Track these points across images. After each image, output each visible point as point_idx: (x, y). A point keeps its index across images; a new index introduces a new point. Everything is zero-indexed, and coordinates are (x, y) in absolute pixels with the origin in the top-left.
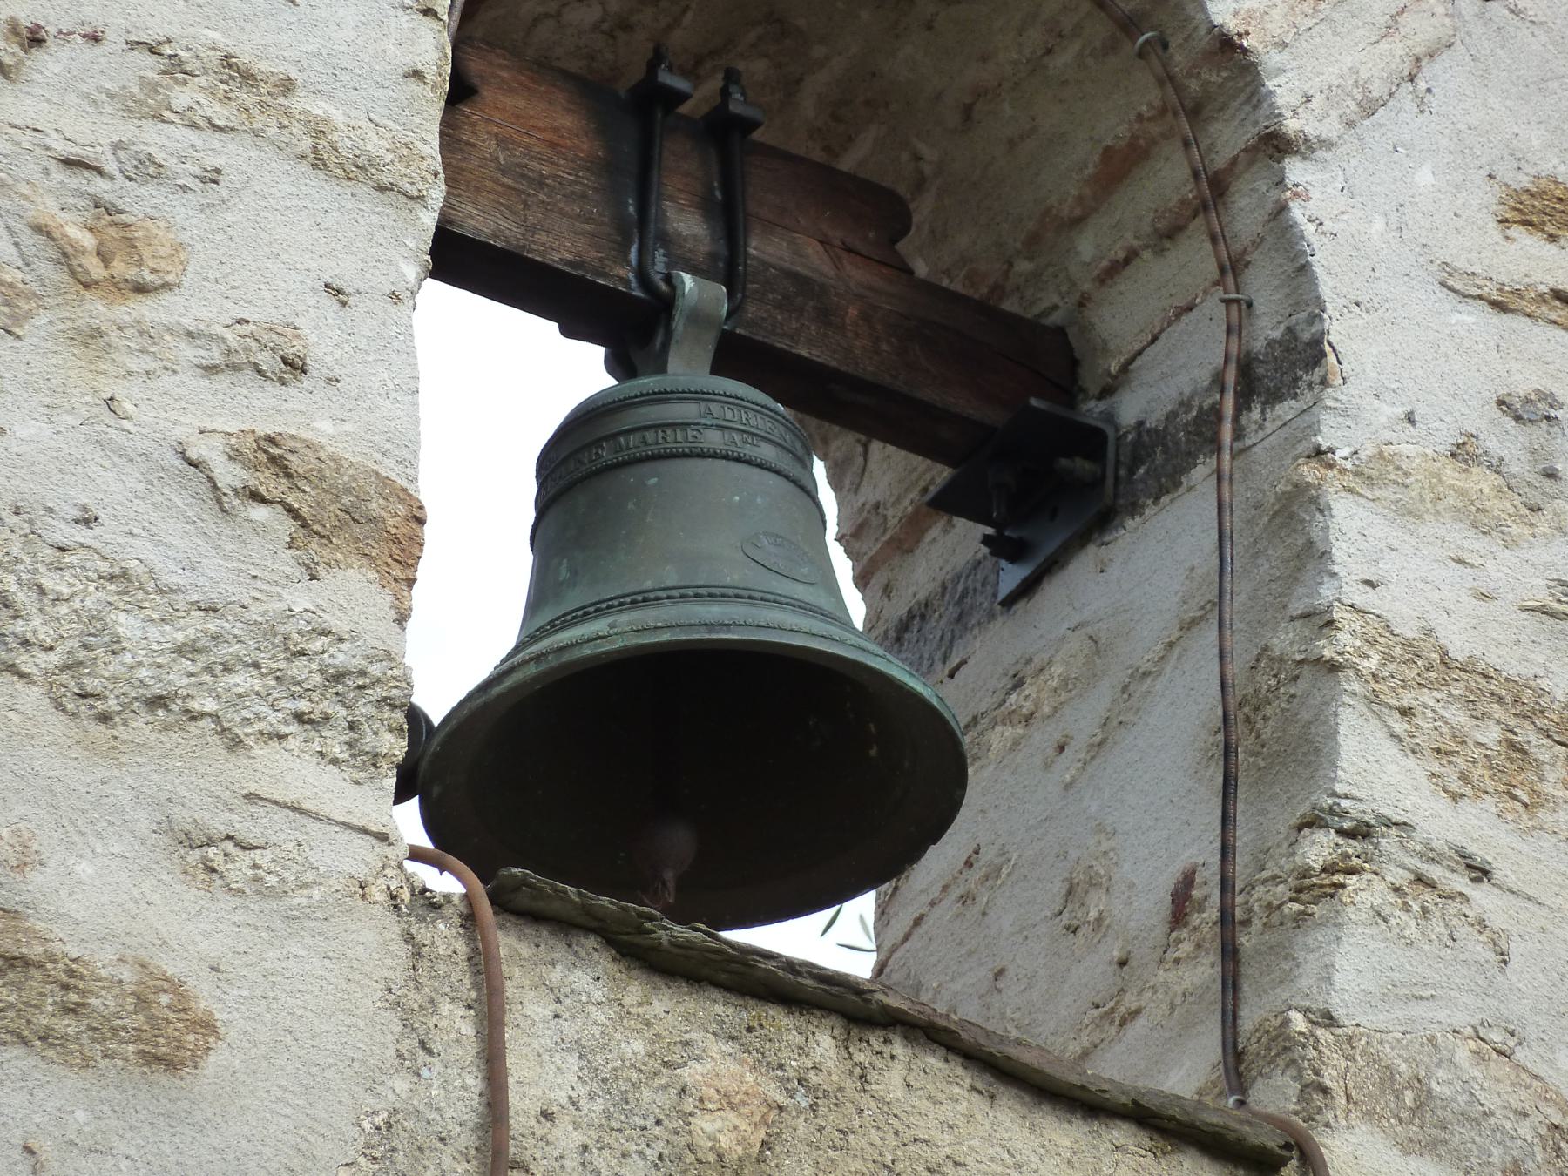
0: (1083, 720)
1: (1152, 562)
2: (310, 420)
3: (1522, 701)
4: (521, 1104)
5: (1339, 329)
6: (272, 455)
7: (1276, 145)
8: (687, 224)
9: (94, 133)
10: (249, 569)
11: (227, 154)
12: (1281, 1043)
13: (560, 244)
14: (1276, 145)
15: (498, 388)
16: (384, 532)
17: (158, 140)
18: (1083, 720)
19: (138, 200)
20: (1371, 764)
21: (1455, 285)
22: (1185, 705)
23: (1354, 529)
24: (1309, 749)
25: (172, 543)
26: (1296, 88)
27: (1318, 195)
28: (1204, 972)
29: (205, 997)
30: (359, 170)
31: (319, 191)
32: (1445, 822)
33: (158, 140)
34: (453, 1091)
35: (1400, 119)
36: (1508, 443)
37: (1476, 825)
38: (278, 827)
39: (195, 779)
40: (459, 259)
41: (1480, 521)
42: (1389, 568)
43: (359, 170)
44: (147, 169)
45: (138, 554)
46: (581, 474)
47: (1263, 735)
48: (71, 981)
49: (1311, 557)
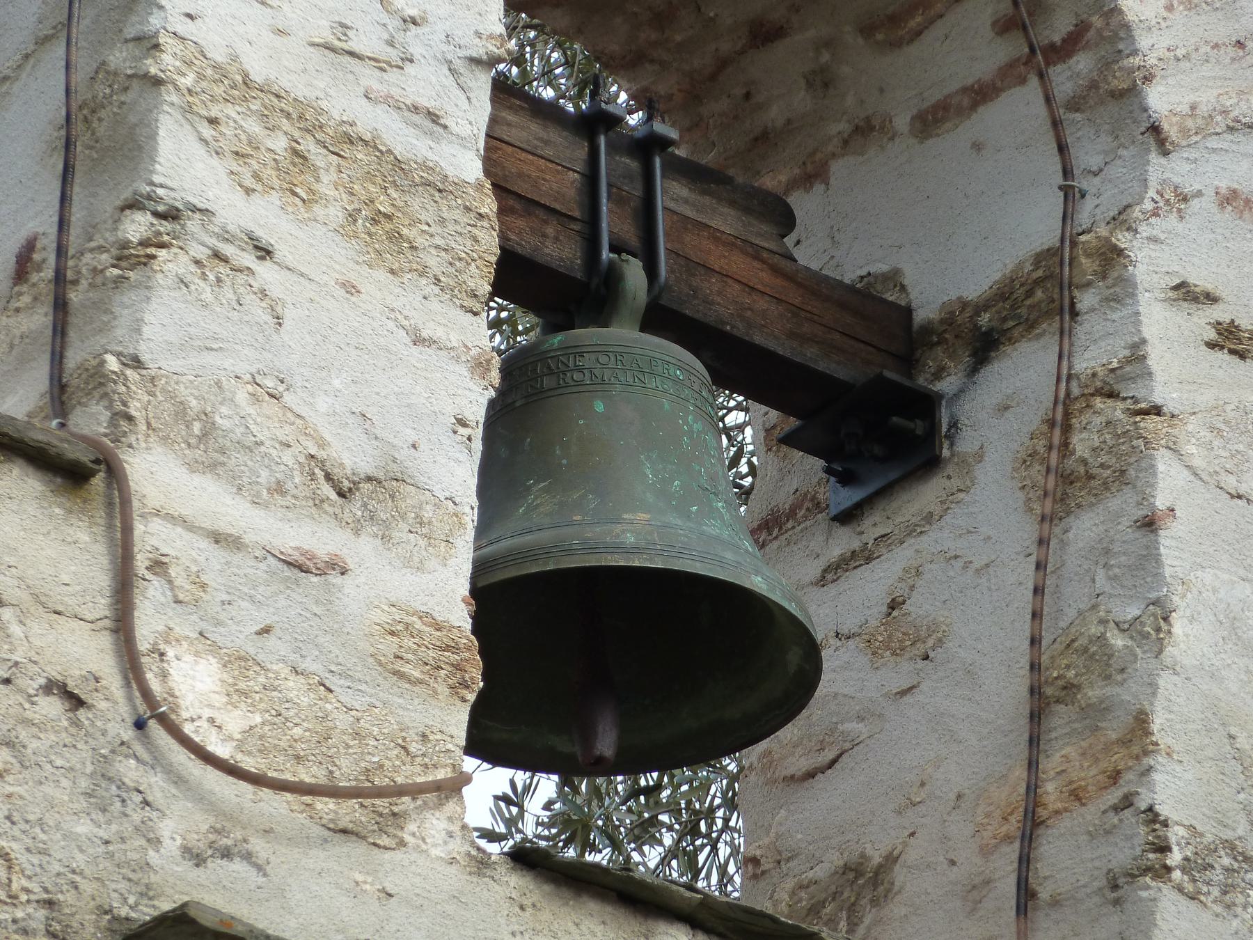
3: (306, 118)
12: (98, 379)
20: (182, 161)
24: (134, 147)
28: (40, 319)
32: (237, 210)
37: (264, 214)
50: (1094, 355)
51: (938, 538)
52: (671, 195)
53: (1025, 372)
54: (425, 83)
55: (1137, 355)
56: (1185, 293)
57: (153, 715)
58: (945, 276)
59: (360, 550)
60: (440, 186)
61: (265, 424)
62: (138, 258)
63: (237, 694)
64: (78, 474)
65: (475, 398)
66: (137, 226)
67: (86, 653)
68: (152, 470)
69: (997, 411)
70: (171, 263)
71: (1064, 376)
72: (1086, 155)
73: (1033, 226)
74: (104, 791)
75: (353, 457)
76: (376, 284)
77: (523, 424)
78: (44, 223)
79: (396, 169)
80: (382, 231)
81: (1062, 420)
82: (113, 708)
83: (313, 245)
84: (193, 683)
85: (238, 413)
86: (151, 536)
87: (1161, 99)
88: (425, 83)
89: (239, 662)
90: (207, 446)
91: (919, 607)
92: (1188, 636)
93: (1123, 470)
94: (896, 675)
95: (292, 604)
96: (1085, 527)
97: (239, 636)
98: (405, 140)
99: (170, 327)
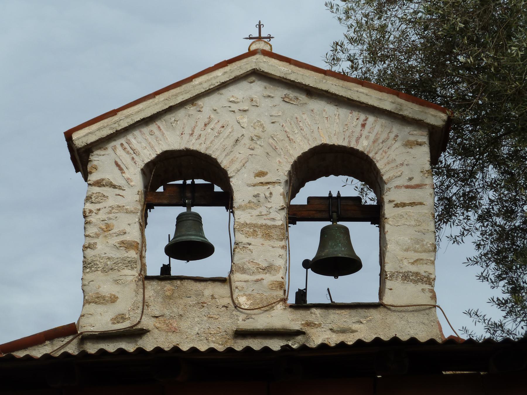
3: (255, 226)
4: (146, 296)
9: (105, 217)
11: (118, 215)
14: (229, 178)
19: (109, 222)
21: (249, 185)
29: (117, 295)
36: (255, 200)
37: (250, 240)
38: (124, 277)
39: (115, 275)
41: (252, 208)
44: (110, 219)
45: (110, 255)
48: (104, 298)
56: (390, 201)
57: (237, 306)
63: (248, 299)
75: (264, 265)
76: (267, 243)
87: (384, 178)
95: (256, 286)
97: (249, 292)
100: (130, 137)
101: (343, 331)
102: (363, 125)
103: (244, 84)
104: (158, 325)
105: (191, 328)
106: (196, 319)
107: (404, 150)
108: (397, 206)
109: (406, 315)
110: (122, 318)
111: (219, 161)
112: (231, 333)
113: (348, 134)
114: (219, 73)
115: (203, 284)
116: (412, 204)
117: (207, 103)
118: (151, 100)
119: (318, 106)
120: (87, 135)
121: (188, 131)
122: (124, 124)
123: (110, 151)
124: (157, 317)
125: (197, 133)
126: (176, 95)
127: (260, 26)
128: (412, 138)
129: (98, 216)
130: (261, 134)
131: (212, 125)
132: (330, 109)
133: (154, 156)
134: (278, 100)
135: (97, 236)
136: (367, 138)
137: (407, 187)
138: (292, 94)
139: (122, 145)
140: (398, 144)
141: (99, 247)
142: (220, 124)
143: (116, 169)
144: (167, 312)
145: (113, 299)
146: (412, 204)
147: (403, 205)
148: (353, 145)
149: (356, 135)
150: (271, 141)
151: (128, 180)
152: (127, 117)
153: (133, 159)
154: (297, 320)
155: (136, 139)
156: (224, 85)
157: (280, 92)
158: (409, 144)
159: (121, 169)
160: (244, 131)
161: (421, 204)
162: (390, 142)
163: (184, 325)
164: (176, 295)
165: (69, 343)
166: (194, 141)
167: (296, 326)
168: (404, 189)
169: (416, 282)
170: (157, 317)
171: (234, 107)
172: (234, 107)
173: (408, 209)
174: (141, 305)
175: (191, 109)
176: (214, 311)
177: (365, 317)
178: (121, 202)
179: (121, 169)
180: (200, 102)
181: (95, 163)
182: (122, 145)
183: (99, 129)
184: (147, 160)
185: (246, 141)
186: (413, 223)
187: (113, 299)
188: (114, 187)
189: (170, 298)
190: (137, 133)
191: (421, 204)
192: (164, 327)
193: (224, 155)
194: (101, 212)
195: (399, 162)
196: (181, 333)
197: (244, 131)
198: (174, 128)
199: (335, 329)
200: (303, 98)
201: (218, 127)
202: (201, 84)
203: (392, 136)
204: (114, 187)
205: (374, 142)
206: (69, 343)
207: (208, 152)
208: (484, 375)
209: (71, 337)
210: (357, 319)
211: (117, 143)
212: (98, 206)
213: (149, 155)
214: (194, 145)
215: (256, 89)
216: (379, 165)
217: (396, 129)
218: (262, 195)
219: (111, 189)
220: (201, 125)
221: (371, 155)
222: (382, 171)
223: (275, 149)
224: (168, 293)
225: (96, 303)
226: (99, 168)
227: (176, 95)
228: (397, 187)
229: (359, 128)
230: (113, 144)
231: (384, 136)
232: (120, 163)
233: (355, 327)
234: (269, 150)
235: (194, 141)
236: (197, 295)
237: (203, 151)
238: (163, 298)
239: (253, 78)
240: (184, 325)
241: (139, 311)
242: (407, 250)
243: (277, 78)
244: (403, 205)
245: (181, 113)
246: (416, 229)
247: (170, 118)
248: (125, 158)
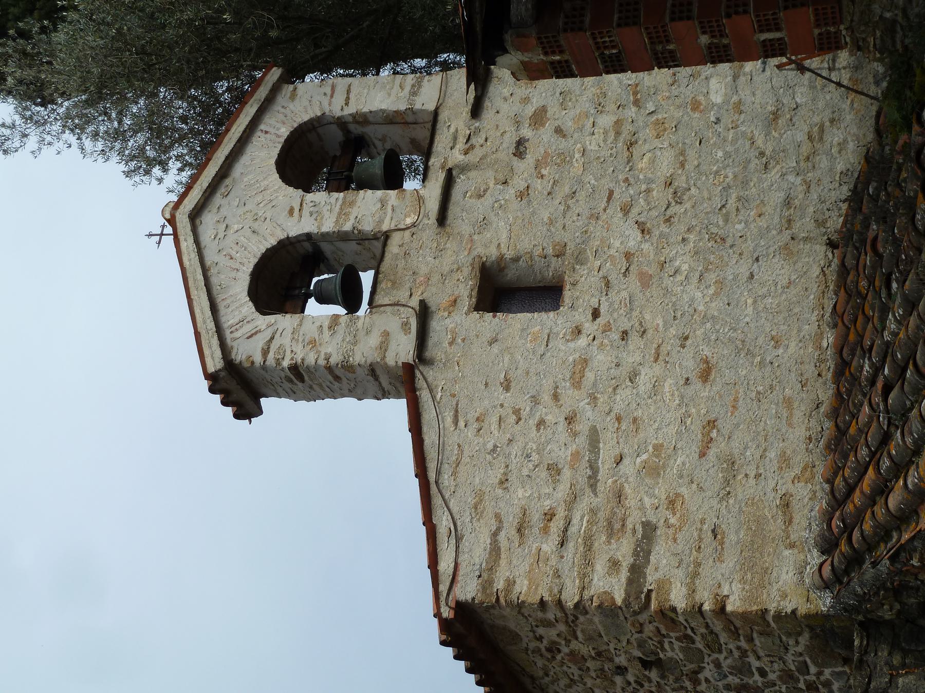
0: (340, 253)
1: (326, 248)
2: (326, 324)
3: (340, 214)
4: (389, 303)
5: (305, 231)
6: (330, 328)
7: (288, 237)
8: (297, 292)
9: (300, 345)
10: (341, 329)
11: (301, 333)
12: (375, 234)
13: (301, 303)
14: (288, 237)
15: (313, 307)
16: (335, 318)
17: (301, 340)
18: (340, 253)
19: (307, 341)
20: (347, 227)
21: (299, 221)
22: (341, 245)
23: (325, 229)
24: (346, 233)
25: (339, 337)
26: (282, 236)
27: (293, 233)
28: (367, 242)
29: (382, 331)
30: (301, 321)
31: (304, 325)
32: (352, 221)
33: (301, 340)
34: (389, 309)
35: (284, 226)
36: (314, 216)
37: (352, 218)
38: (365, 325)
39: (361, 334)
40: (303, 311)
41: (322, 218)
42: (328, 226)
43: (301, 321)
44: (303, 340)
45: (341, 339)
46: (322, 300)
47: (344, 237)
48: (382, 343)
49: (328, 233)
50: (351, 119)
51: (372, 135)
52: (335, 170)
53: (352, 127)
54: (333, 200)
55: (350, 115)
56: (342, 109)
57: (414, 225)
58: (339, 135)
59: (390, 203)
60: (345, 198)
61: (377, 216)
62: (360, 231)
63: (409, 216)
64: (387, 236)
65: (370, 192)
66: (356, 232)
67: (407, 233)
68: (385, 228)
69: (356, 129)
70: (360, 228)
71: (353, 123)
72: (326, 122)
73: (334, 128)
74: (423, 230)
75: (379, 205)
76: (358, 204)
77: (363, 185)
78: (354, 242)
79: (344, 203)
80: (352, 204)
81: (357, 122)
82: (413, 230)
83: (354, 212)
84: (409, 221)
85: (376, 218)
86: (393, 227)
87: (319, 114)
88: (333, 200)
89: (406, 216)
90: (381, 221)
91: (380, 137)
92: (384, 107)
93: (364, 115)
94: (388, 139)
95: (398, 211)
96: (371, 119)
97: (403, 216)
98: (340, 202)
99: (368, 226)
100: (225, 326)
101: (455, 138)
102: (266, 132)
103: (201, 229)
104: (420, 292)
105: (427, 264)
106: (420, 259)
107: (297, 101)
108: (347, 104)
109: (449, 90)
110: (405, 326)
111: (269, 246)
112: (439, 230)
113: (271, 144)
114: (183, 245)
115: (386, 254)
116: (348, 92)
117: (209, 259)
118: (194, 303)
119: (238, 169)
120: (213, 358)
121: (233, 274)
122: (211, 325)
123: (235, 344)
124: (411, 295)
125: (237, 266)
126: (195, 280)
127: (150, 235)
128: (289, 95)
129: (299, 352)
130: (253, 214)
131: (233, 253)
132: (244, 160)
133: (251, 304)
134: (224, 202)
135: (318, 352)
136: (278, 129)
137: (332, 96)
138: (222, 190)
139: (231, 332)
140: (291, 106)
141: (329, 350)
142: (234, 246)
143: (255, 337)
144: (408, 286)
145: (386, 334)
146: (348, 92)
147: (348, 99)
148: (282, 140)
149: (273, 137)
150: (261, 205)
151: (269, 326)
152: (205, 322)
153: (248, 322)
154: (437, 177)
155: (229, 319)
156: (197, 242)
157: (218, 199)
158: (293, 96)
159: (256, 333)
160: (246, 227)
161: (350, 86)
162: (287, 111)
163: (424, 270)
164: (392, 277)
165: (422, 373)
166: (244, 268)
167: (442, 176)
168: (333, 100)
169: (420, 87)
170: (411, 295)
171: (221, 235)
172: (221, 235)
173: (352, 96)
174: (396, 308)
175: (213, 271)
176: (414, 245)
177: (445, 122)
178: (289, 331)
179: (256, 333)
180: (208, 262)
181: (244, 357)
182: (231, 332)
183: (210, 347)
184: (254, 309)
185: (256, 226)
186: (366, 91)
187: (386, 334)
188: (272, 338)
189: (394, 283)
190: (223, 319)
191: (350, 86)
192: (422, 288)
193: (264, 242)
194: (294, 349)
195: (308, 103)
196: (430, 273)
197: (246, 227)
198: (228, 287)
199: (451, 145)
200: (228, 181)
201: (236, 248)
202: (190, 260)
203: (283, 110)
204: (272, 338)
205: (284, 123)
206: (422, 373)
207: (259, 255)
208: (921, 560)
209: (417, 372)
210: (445, 130)
211: (228, 336)
212: (288, 353)
213: (249, 308)
214: (249, 268)
215: (208, 220)
216: (306, 118)
217: (277, 107)
218: (312, 209)
219: (274, 342)
220: (231, 263)
221: (296, 125)
222: (313, 115)
223: (271, 201)
224: (389, 284)
225: (386, 350)
226: (251, 353)
227: (195, 280)
228: (330, 105)
229: (268, 136)
230: (229, 341)
231: (281, 117)
232: (249, 334)
233: (452, 130)
234: (270, 205)
235: (244, 268)
236: (397, 259)
237: (256, 260)
238: (393, 289)
239: (198, 221)
240: (424, 270)
241: (402, 309)
242: (389, 95)
243: (202, 200)
244: (348, 99)
245: (214, 280)
246: (371, 89)
247: (216, 289)
248: (247, 329)
